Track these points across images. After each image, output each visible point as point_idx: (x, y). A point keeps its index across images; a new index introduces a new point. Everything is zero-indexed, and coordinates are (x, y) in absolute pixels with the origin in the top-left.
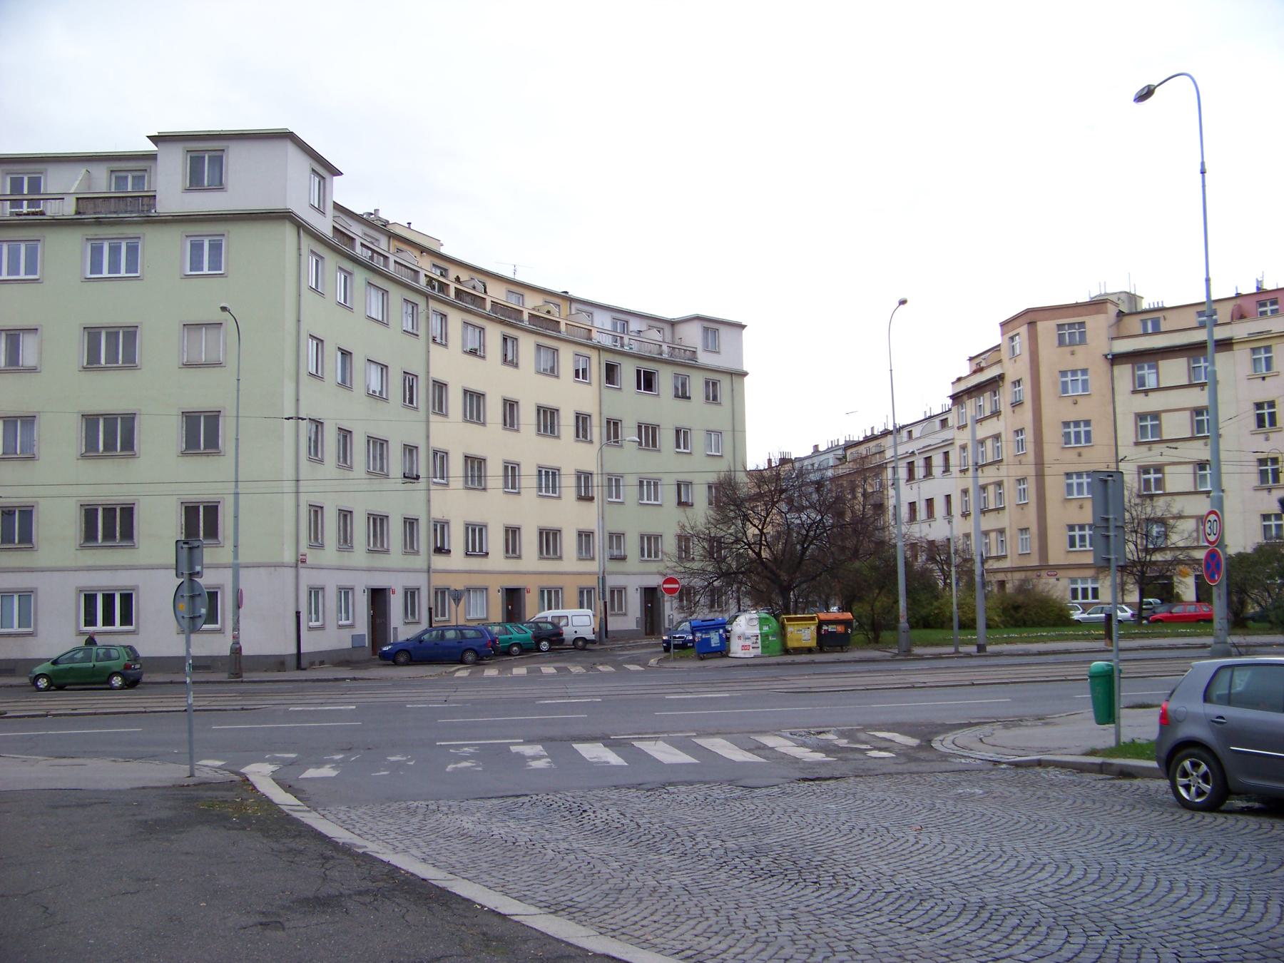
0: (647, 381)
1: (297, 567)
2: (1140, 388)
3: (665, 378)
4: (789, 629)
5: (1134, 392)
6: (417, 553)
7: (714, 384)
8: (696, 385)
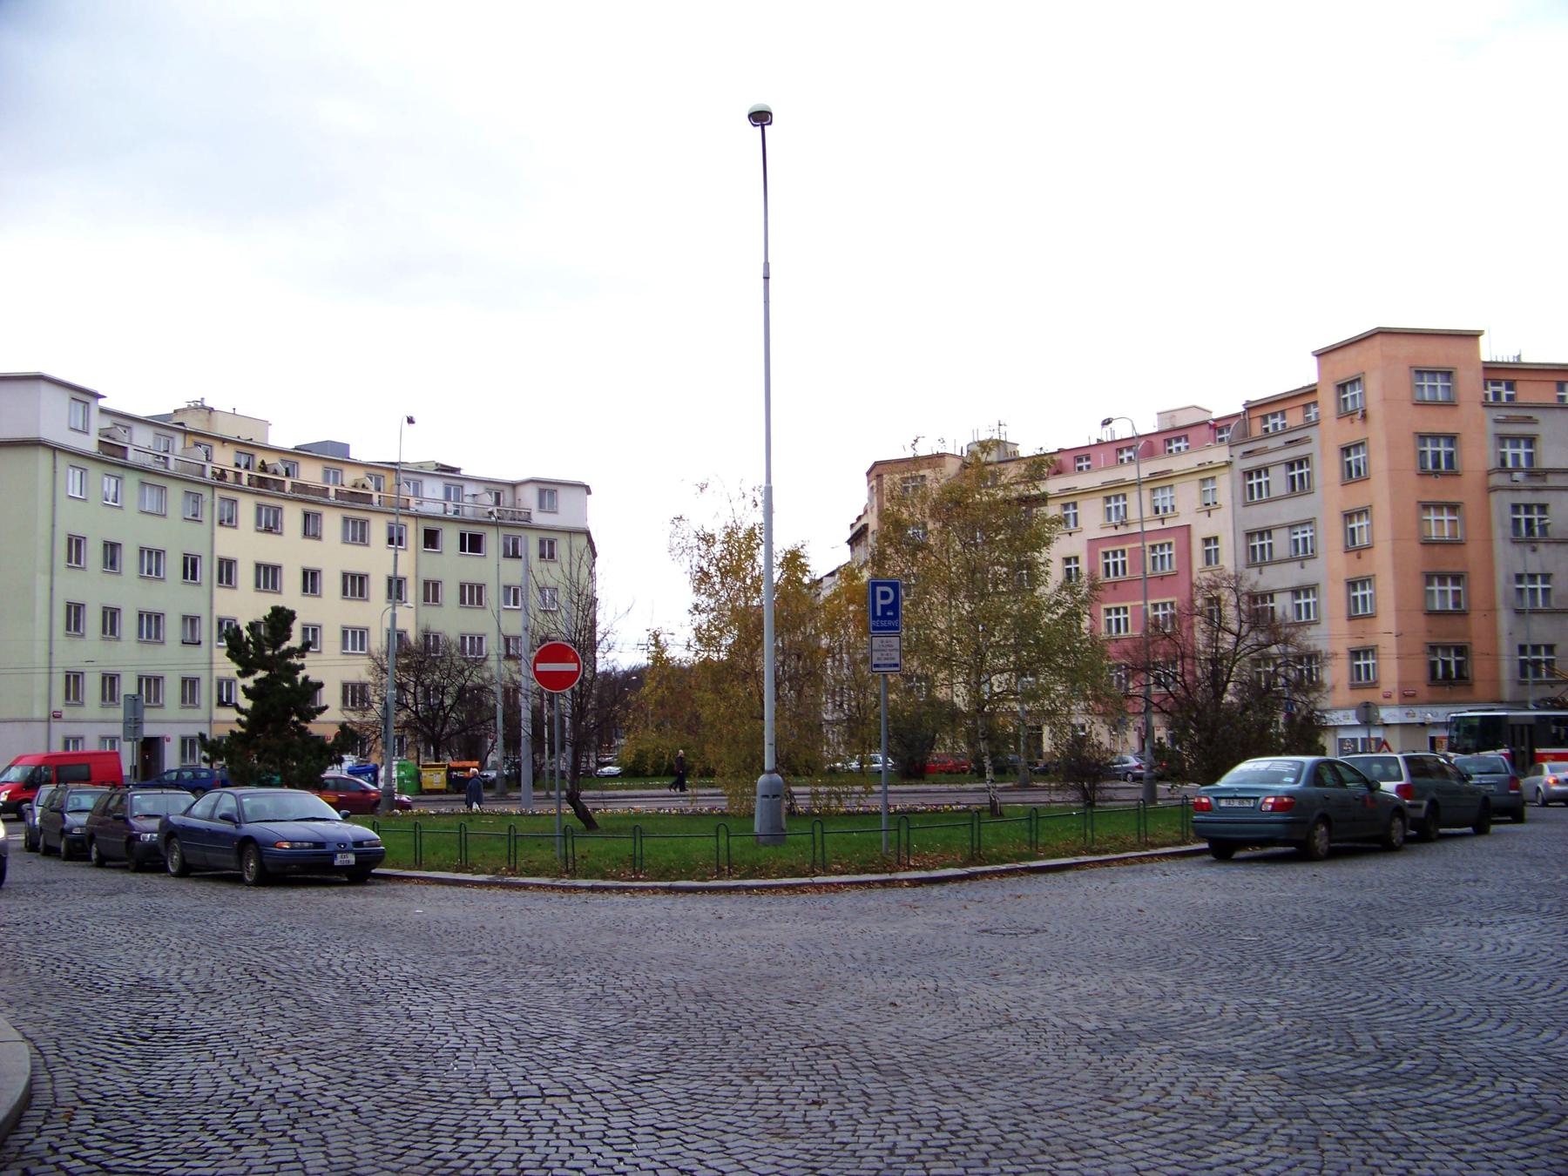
0: (473, 544)
1: (49, 721)
3: (493, 541)
4: (424, 774)
6: (198, 707)
7: (551, 543)
8: (531, 544)
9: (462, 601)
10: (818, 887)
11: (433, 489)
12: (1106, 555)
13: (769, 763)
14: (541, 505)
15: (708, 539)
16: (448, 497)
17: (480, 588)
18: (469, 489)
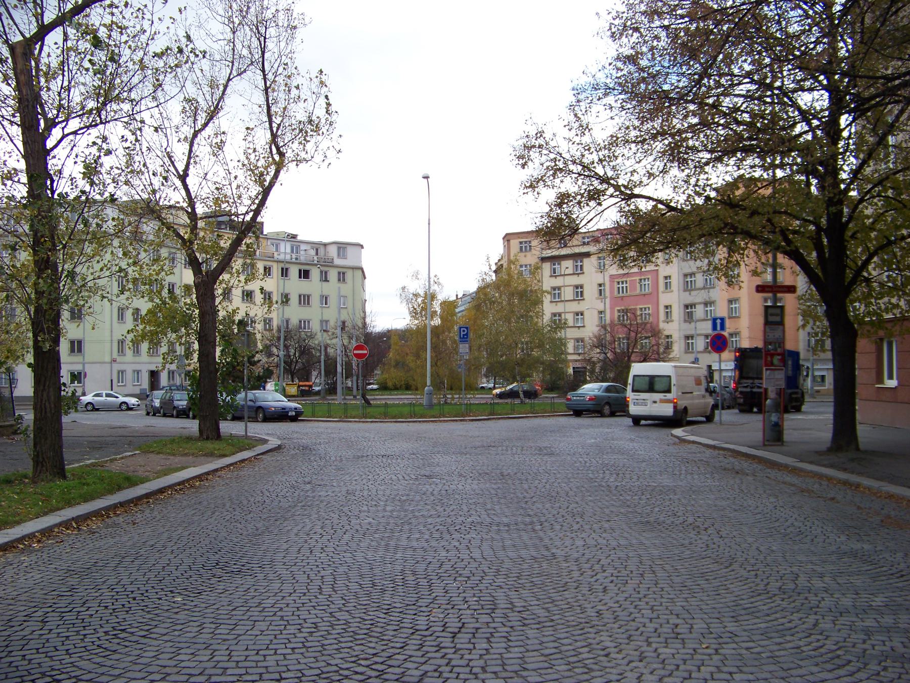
0: (305, 274)
2: (554, 274)
3: (315, 273)
5: (551, 276)
7: (344, 273)
8: (333, 275)
9: (300, 303)
10: (441, 421)
11: (285, 248)
12: (618, 283)
13: (428, 383)
14: (339, 255)
15: (416, 295)
16: (292, 252)
17: (308, 297)
18: (303, 247)
